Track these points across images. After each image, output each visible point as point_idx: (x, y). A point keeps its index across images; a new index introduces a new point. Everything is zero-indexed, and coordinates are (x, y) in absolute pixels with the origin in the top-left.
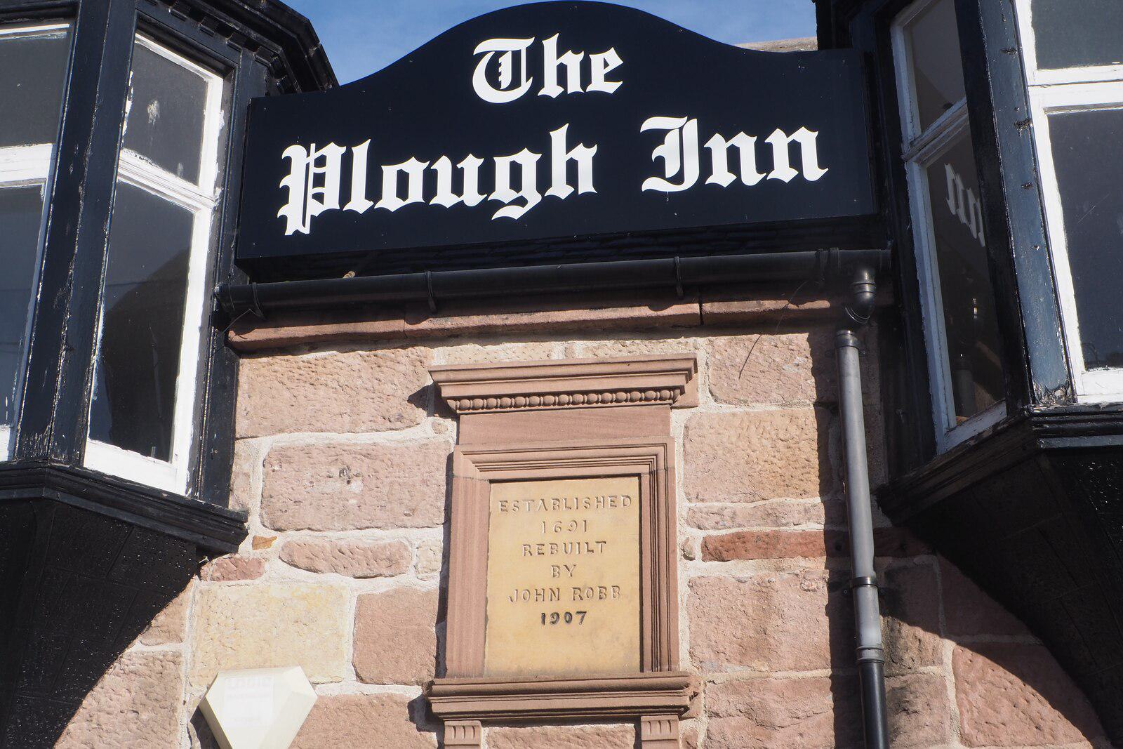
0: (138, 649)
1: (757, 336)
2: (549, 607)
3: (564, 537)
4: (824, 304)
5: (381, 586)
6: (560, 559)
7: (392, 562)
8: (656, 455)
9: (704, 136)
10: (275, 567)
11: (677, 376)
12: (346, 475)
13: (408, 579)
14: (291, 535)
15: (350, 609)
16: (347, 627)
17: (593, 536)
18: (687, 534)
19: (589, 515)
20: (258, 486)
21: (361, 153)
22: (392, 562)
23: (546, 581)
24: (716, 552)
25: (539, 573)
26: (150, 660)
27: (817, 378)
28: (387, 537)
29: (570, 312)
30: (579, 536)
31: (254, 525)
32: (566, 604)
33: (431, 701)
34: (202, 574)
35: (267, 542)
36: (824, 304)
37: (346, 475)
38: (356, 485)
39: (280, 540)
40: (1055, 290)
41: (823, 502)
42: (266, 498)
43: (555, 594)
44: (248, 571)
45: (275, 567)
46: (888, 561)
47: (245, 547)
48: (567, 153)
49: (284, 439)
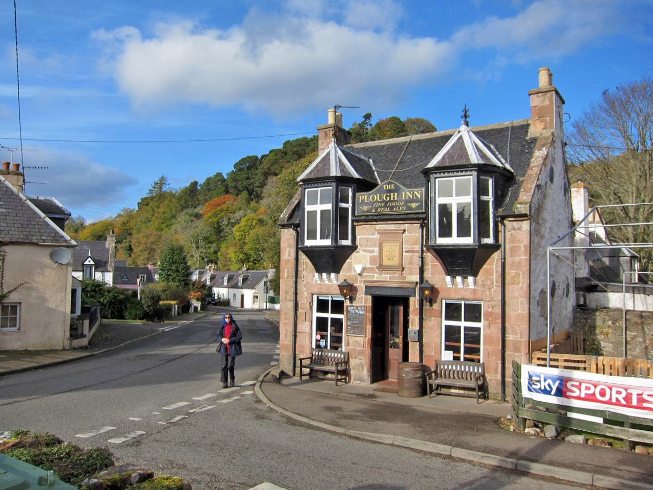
0: (348, 260)
4: (445, 219)
5: (372, 254)
7: (373, 252)
8: (313, 294)
12: (368, 241)
13: (375, 254)
15: (369, 257)
16: (369, 259)
18: (404, 250)
20: (358, 242)
21: (366, 201)
22: (373, 252)
24: (406, 252)
25: (388, 254)
26: (349, 262)
28: (371, 249)
29: (56, 226)
31: (359, 247)
32: (391, 258)
33: (340, 296)
34: (462, 209)
36: (445, 219)
37: (368, 241)
38: (369, 243)
39: (361, 249)
42: (359, 243)
45: (361, 252)
47: (358, 249)
48: (329, 152)
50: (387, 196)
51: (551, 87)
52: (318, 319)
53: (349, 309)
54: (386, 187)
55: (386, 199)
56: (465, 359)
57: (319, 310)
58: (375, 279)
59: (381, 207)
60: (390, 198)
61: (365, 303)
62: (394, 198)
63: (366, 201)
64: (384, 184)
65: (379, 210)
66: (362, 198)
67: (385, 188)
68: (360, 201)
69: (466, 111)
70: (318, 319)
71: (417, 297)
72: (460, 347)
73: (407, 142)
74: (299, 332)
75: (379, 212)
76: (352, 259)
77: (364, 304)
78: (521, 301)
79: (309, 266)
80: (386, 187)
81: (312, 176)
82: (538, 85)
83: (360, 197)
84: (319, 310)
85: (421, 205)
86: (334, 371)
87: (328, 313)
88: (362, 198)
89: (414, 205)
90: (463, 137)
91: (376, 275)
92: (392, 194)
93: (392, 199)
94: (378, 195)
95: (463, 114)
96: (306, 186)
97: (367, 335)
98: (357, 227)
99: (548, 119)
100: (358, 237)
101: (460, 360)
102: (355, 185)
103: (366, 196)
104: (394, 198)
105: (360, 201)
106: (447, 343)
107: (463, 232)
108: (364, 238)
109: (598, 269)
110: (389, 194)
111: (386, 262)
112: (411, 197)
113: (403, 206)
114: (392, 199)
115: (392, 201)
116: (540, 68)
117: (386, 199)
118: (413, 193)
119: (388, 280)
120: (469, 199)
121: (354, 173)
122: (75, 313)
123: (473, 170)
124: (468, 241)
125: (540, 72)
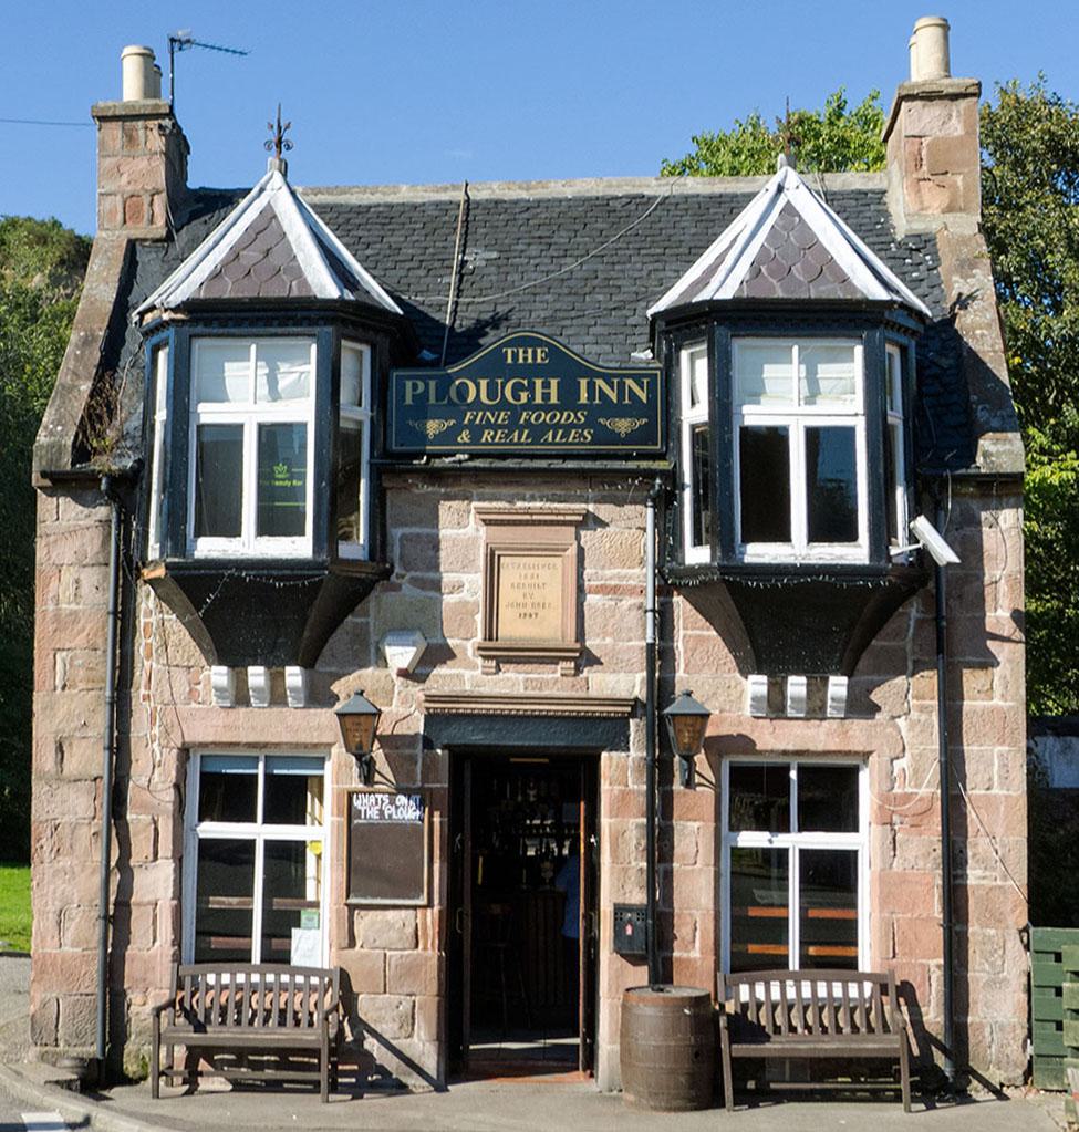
1: (131, 783)
2: (523, 611)
3: (529, 581)
6: (527, 590)
9: (431, 815)
10: (407, 588)
11: (107, 724)
14: (413, 574)
17: (541, 581)
19: (540, 572)
23: (521, 600)
25: (517, 596)
27: (962, 1019)
30: (535, 581)
32: (529, 610)
35: (403, 577)
40: (903, 390)
41: (962, 744)
42: (401, 557)
43: (525, 605)
44: (397, 588)
45: (407, 588)
46: (760, 854)
49: (407, 530)
50: (516, 389)
51: (151, 102)
52: (848, 823)
53: (357, 803)
54: (515, 356)
55: (517, 397)
56: (806, 962)
57: (847, 860)
58: (468, 688)
59: (495, 427)
60: (532, 398)
61: (423, 781)
62: (546, 396)
63: (432, 400)
64: (507, 344)
65: (487, 435)
66: (415, 387)
67: (510, 360)
68: (409, 401)
69: (280, 128)
70: (848, 823)
71: (636, 751)
72: (786, 919)
73: (656, 197)
74: (139, 905)
75: (487, 443)
76: (366, 614)
77: (419, 784)
78: (1001, 755)
79: (173, 639)
80: (515, 356)
81: (228, 290)
82: (122, 98)
83: (409, 384)
84: (847, 860)
85: (652, 425)
86: (316, 1046)
87: (254, 820)
88: (415, 387)
89: (623, 426)
90: (793, 203)
91: (467, 674)
92: (538, 382)
93: (538, 400)
94: (483, 383)
95: (272, 136)
96: (200, 329)
97: (436, 901)
98: (389, 494)
99: (959, 179)
100: (396, 533)
101: (786, 965)
102: (384, 342)
103: (432, 384)
104: (546, 396)
105: (409, 401)
106: (776, 913)
107: (831, 522)
108: (418, 535)
109: (198, 610)
110: (525, 382)
111: (512, 628)
112: (643, 396)
113: (583, 427)
114: (538, 400)
115: (537, 407)
116: (917, 19)
117: (517, 397)
118: (622, 385)
119: (520, 691)
120: (301, 409)
121: (380, 296)
122: (319, 1050)
123: (258, 319)
124: (299, 547)
125: (125, 61)
